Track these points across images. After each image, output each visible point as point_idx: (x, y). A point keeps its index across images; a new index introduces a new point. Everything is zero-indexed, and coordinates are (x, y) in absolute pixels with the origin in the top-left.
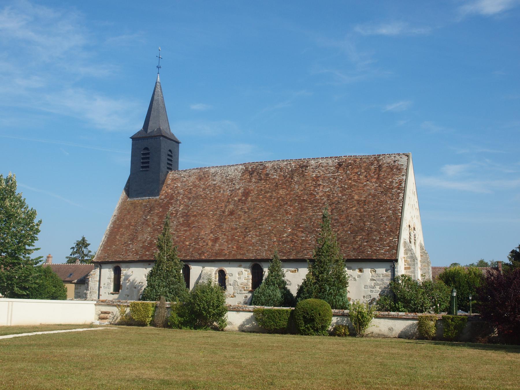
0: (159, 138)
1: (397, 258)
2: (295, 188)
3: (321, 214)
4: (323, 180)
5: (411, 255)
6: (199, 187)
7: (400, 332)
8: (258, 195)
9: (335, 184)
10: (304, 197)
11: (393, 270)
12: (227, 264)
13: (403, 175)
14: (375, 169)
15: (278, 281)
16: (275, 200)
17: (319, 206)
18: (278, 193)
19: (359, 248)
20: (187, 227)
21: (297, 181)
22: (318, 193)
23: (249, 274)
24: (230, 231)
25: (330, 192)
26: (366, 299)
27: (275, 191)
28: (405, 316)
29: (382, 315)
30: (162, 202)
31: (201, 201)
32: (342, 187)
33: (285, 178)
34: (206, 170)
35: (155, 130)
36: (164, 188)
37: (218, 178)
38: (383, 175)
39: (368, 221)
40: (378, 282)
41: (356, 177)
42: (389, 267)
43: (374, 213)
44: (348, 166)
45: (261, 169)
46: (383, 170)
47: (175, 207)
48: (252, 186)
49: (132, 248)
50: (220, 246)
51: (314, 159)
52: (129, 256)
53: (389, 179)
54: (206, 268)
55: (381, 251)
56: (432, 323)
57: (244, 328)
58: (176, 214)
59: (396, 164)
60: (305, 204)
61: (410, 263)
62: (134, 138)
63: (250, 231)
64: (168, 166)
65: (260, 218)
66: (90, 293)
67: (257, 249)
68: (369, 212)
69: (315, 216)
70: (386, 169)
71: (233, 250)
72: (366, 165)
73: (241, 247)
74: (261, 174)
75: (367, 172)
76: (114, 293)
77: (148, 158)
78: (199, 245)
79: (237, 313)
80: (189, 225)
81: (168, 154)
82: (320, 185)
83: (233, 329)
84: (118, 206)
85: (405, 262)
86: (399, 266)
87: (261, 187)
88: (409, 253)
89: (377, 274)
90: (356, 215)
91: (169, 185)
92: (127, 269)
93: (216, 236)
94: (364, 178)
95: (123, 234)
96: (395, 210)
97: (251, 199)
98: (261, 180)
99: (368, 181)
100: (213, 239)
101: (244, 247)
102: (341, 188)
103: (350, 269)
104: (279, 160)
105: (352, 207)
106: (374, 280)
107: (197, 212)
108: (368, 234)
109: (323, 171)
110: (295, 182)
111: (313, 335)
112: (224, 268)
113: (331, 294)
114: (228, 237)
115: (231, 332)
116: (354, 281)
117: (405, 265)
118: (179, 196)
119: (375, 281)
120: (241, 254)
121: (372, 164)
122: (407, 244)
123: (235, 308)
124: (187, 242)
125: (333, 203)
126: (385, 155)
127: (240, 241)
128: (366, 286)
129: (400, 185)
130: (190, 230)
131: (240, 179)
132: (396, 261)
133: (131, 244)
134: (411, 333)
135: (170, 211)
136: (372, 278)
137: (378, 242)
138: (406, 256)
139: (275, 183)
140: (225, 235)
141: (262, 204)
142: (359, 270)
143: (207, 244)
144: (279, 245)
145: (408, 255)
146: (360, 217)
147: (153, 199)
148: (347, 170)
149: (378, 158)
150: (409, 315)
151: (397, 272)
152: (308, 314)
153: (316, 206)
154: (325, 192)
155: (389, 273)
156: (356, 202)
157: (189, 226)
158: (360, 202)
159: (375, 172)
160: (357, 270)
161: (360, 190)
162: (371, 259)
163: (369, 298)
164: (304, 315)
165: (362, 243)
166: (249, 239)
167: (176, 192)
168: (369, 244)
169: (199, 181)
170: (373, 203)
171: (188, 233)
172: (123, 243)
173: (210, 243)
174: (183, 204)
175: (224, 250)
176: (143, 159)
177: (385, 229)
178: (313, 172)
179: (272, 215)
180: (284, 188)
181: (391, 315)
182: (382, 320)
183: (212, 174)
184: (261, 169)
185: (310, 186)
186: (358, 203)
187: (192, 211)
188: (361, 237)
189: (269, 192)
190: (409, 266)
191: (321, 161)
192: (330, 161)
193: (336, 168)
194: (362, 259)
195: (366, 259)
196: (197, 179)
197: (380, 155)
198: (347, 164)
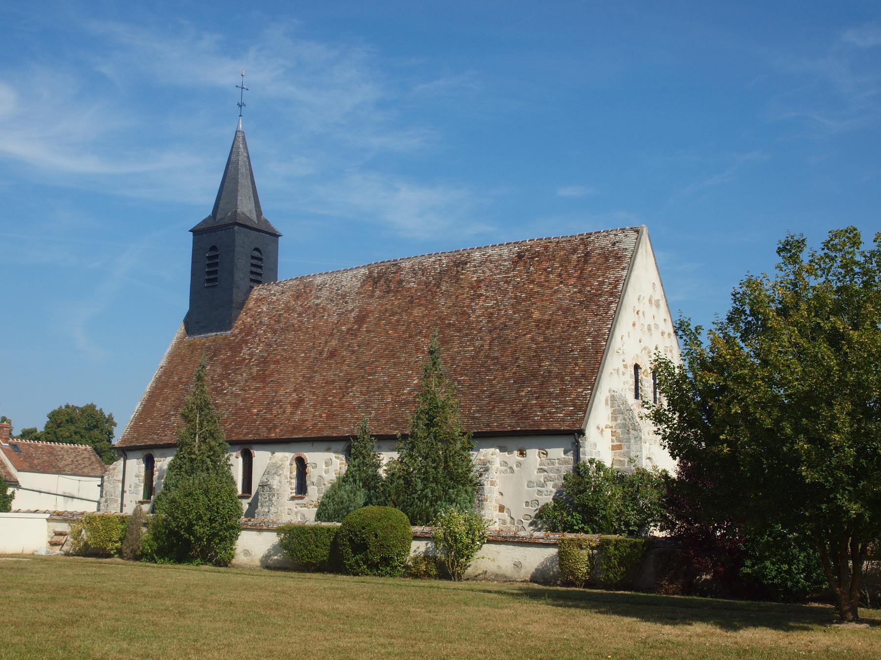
0: (233, 228)
1: (582, 427)
2: (440, 304)
3: (472, 348)
4: (487, 286)
5: (623, 421)
6: (294, 310)
7: (533, 570)
8: (379, 320)
9: (505, 293)
10: (450, 320)
11: (576, 449)
12: (309, 445)
13: (623, 269)
14: (578, 261)
15: (364, 475)
16: (404, 328)
17: (471, 334)
18: (411, 314)
19: (521, 410)
20: (261, 382)
21: (445, 291)
22: (474, 311)
23: (343, 463)
24: (323, 387)
25: (494, 308)
26: (530, 507)
27: (406, 311)
28: (543, 538)
29: (503, 537)
30: (234, 340)
31: (291, 336)
32: (516, 297)
33: (427, 287)
34: (308, 280)
35: (229, 214)
36: (243, 315)
37: (325, 293)
38: (590, 271)
39: (547, 358)
40: (551, 475)
41: (543, 277)
42: (570, 444)
43: (560, 343)
44: (533, 258)
45: (393, 273)
46: (592, 261)
47: (250, 348)
48: (374, 304)
49: (174, 423)
50: (302, 414)
51: (480, 248)
52: (166, 435)
53: (599, 277)
54: (277, 454)
55: (559, 415)
56: (584, 554)
57: (269, 561)
58: (250, 360)
59: (616, 248)
60: (449, 332)
61: (621, 436)
62: (195, 231)
63: (353, 386)
64: (253, 277)
65: (373, 362)
66: (106, 501)
67: (357, 419)
68: (553, 342)
69: (462, 353)
70: (598, 259)
71: (320, 421)
72: (565, 254)
73: (334, 415)
74: (391, 281)
75: (562, 266)
76: (144, 502)
77: (216, 264)
78: (272, 414)
79: (258, 533)
80: (264, 379)
81: (252, 256)
82: (482, 295)
83: (251, 564)
84: (169, 350)
85: (612, 436)
86: (587, 443)
87: (386, 304)
88: (620, 417)
89: (550, 459)
90: (529, 348)
91: (250, 309)
92: (162, 459)
93: (300, 397)
94: (556, 278)
95: (166, 399)
96: (598, 336)
97: (367, 327)
98: (388, 292)
99: (561, 283)
100: (294, 401)
101: (338, 415)
102: (515, 299)
103: (505, 451)
104: (424, 255)
105: (525, 334)
106: (545, 471)
107: (282, 356)
108: (542, 384)
109: (490, 270)
110: (442, 293)
111: (367, 575)
112: (305, 454)
113: (426, 496)
114: (318, 397)
115: (244, 570)
116: (511, 474)
117: (613, 441)
118: (260, 328)
119: (546, 473)
120: (330, 427)
121: (575, 251)
122: (616, 400)
123: (255, 525)
124: (255, 408)
125: (496, 328)
126: (599, 232)
127: (334, 404)
128: (531, 482)
129: (615, 287)
130: (264, 387)
131: (356, 293)
132: (582, 433)
133: (173, 415)
134: (554, 572)
135: (242, 354)
136: (540, 467)
137: (555, 398)
138: (614, 424)
139: (409, 297)
140: (314, 394)
141: (382, 336)
142: (519, 452)
143: (284, 412)
144: (394, 408)
145: (619, 421)
146: (535, 351)
147: (222, 335)
148: (531, 265)
149: (587, 238)
150: (551, 536)
151: (584, 454)
152: (356, 535)
153: (467, 335)
154: (488, 307)
155: (570, 457)
156: (534, 324)
157: (263, 380)
158: (540, 323)
159: (577, 265)
160: (516, 453)
161: (546, 300)
162: (537, 430)
163: (535, 507)
164: (351, 538)
165: (528, 400)
166: (348, 400)
167: (258, 321)
168: (541, 402)
169: (295, 300)
170: (561, 325)
171: (260, 393)
172: (163, 414)
173: (289, 410)
174: (263, 342)
175: (307, 420)
176: (209, 266)
177: (573, 373)
178: (475, 272)
179: (394, 355)
180: (421, 305)
181: (519, 537)
182: (502, 548)
183: (317, 286)
184: (393, 273)
185: (465, 299)
186: (537, 326)
187: (274, 354)
188: (529, 389)
189: (397, 313)
190: (619, 443)
191: (490, 252)
192: (505, 252)
193: (513, 262)
194: (523, 431)
195: (528, 430)
196: (293, 296)
197: (591, 234)
198: (532, 254)
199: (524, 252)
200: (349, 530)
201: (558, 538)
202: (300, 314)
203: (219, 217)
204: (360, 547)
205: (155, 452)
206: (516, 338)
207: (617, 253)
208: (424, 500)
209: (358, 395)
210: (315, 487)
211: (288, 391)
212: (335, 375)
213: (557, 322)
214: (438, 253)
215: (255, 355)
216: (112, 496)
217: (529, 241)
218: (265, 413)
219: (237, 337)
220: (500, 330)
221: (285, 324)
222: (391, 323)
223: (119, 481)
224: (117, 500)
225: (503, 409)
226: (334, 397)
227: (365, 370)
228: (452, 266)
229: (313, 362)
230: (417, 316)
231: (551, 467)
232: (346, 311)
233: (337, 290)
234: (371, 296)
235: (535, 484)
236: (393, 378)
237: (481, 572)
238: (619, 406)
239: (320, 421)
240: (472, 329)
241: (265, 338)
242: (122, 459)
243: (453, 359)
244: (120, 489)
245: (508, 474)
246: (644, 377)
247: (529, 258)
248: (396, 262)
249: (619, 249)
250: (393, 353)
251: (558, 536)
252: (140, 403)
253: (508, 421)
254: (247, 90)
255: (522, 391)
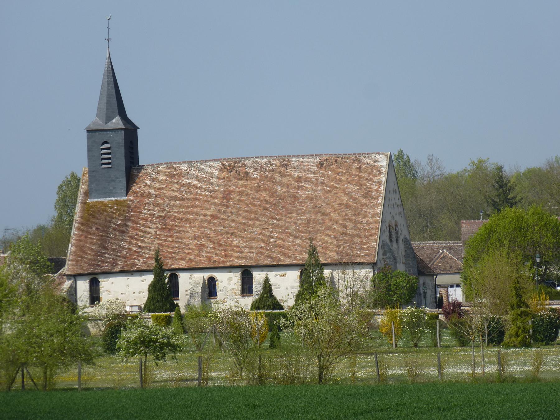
109: (304, 171)
129: (379, 187)
154: (309, 194)
246: (392, 231)
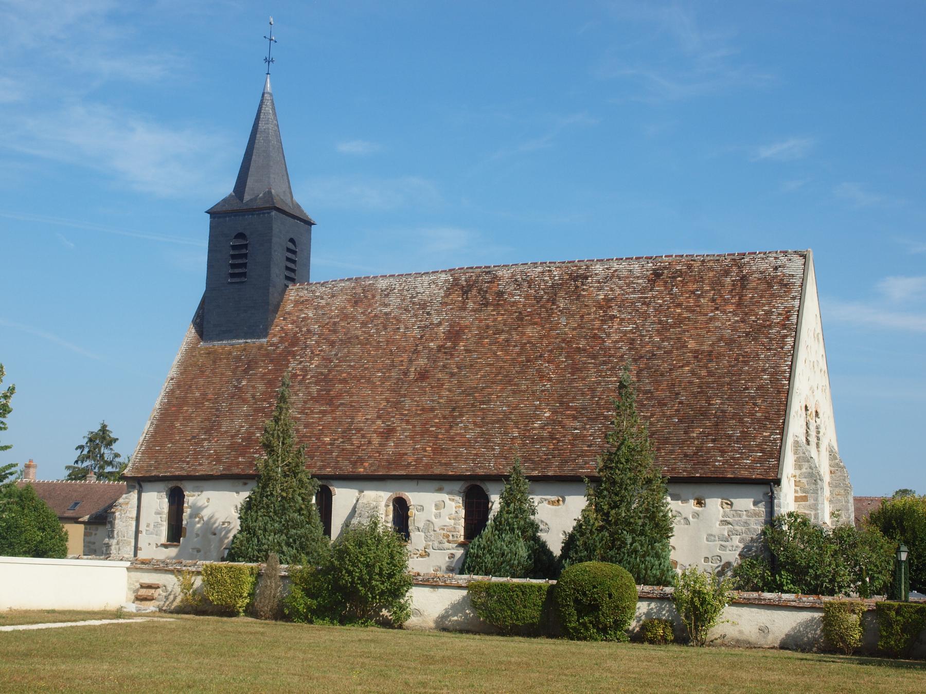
0: (269, 213)
1: (779, 477)
2: (560, 323)
4: (620, 307)
6: (354, 318)
7: (783, 636)
8: (480, 338)
9: (645, 316)
12: (413, 484)
13: (794, 298)
14: (733, 285)
15: (522, 522)
16: (517, 349)
17: (611, 362)
19: (696, 454)
20: (327, 404)
23: (459, 507)
25: (634, 333)
26: (710, 563)
27: (516, 329)
28: (795, 601)
29: (744, 598)
30: (274, 350)
31: (357, 349)
32: (660, 322)
33: (538, 302)
36: (279, 319)
37: (394, 300)
39: (716, 395)
40: (737, 528)
45: (488, 282)
46: (751, 286)
48: (468, 319)
49: (209, 449)
50: (396, 446)
51: (602, 260)
52: (200, 464)
53: (764, 305)
54: (366, 493)
55: (745, 461)
56: (854, 618)
57: (447, 623)
58: (304, 376)
59: (779, 274)
60: (581, 358)
63: (461, 415)
65: (483, 388)
66: (118, 543)
67: (476, 455)
68: (719, 377)
69: (602, 384)
70: (758, 284)
71: (425, 456)
72: (715, 276)
73: (442, 449)
74: (486, 292)
75: (715, 290)
78: (352, 444)
82: (615, 317)
84: (178, 357)
87: (486, 320)
88: (806, 465)
89: (735, 511)
90: (690, 383)
91: (289, 313)
92: (196, 493)
93: (388, 426)
94: (710, 304)
95: (189, 419)
96: (776, 373)
99: (717, 309)
101: (448, 449)
102: (659, 324)
104: (527, 264)
105: (682, 366)
106: (729, 523)
107: (349, 374)
109: (620, 288)
110: (560, 311)
111: (596, 640)
112: (406, 494)
113: (636, 551)
114: (414, 426)
116: (686, 526)
117: (796, 491)
118: (310, 338)
119: (730, 526)
120: (441, 464)
121: (727, 273)
124: (326, 436)
125: (641, 357)
127: (440, 436)
128: (712, 535)
129: (788, 318)
131: (441, 303)
134: (808, 638)
135: (290, 369)
136: (723, 519)
137: (737, 442)
138: (798, 472)
139: (516, 312)
140: (408, 422)
141: (488, 358)
142: (696, 501)
145: (804, 470)
146: (700, 387)
147: (254, 343)
150: (804, 599)
151: (779, 506)
152: (584, 594)
153: (605, 363)
155: (762, 508)
156: (691, 354)
157: (330, 402)
159: (732, 290)
160: (692, 502)
161: (701, 328)
162: (722, 478)
163: (716, 563)
164: (577, 597)
165: (702, 443)
166: (459, 431)
168: (719, 445)
170: (727, 358)
171: (329, 418)
172: (189, 438)
173: (376, 440)
175: (406, 454)
177: (753, 415)
183: (382, 291)
184: (488, 282)
185: (593, 320)
186: (696, 357)
188: (701, 430)
190: (804, 494)
191: (616, 266)
192: (636, 267)
193: (649, 281)
194: (703, 477)
195: (711, 477)
196: (349, 301)
197: (744, 254)
199: (661, 270)
200: (575, 589)
201: (813, 601)
202: (364, 324)
203: (247, 197)
204: (593, 608)
205: (184, 485)
206: (671, 369)
207: (782, 280)
208: (633, 556)
209: (471, 426)
210: (423, 534)
211: (369, 417)
212: (433, 401)
213: (720, 356)
214: (546, 263)
215: (310, 371)
216: (124, 537)
217: (666, 256)
218: (342, 442)
219: (278, 347)
220: (648, 359)
221: (345, 334)
222: (498, 342)
223: (132, 518)
224: (130, 542)
225: (672, 452)
226: (438, 427)
227: (475, 398)
228: (567, 279)
229: (397, 383)
230: (533, 336)
231: (736, 519)
232: (431, 324)
233: (410, 298)
234: (463, 308)
235: (717, 537)
236: (516, 408)
237: (719, 636)
238: (804, 453)
239: (425, 456)
240: (610, 356)
241: (319, 351)
242: (136, 491)
243: (592, 390)
244: (134, 528)
245: (682, 526)
247: (670, 277)
248: (488, 270)
249: (784, 275)
250: (509, 378)
251: (812, 598)
252: (149, 423)
253: (681, 465)
254: (276, 42)
255: (693, 432)
